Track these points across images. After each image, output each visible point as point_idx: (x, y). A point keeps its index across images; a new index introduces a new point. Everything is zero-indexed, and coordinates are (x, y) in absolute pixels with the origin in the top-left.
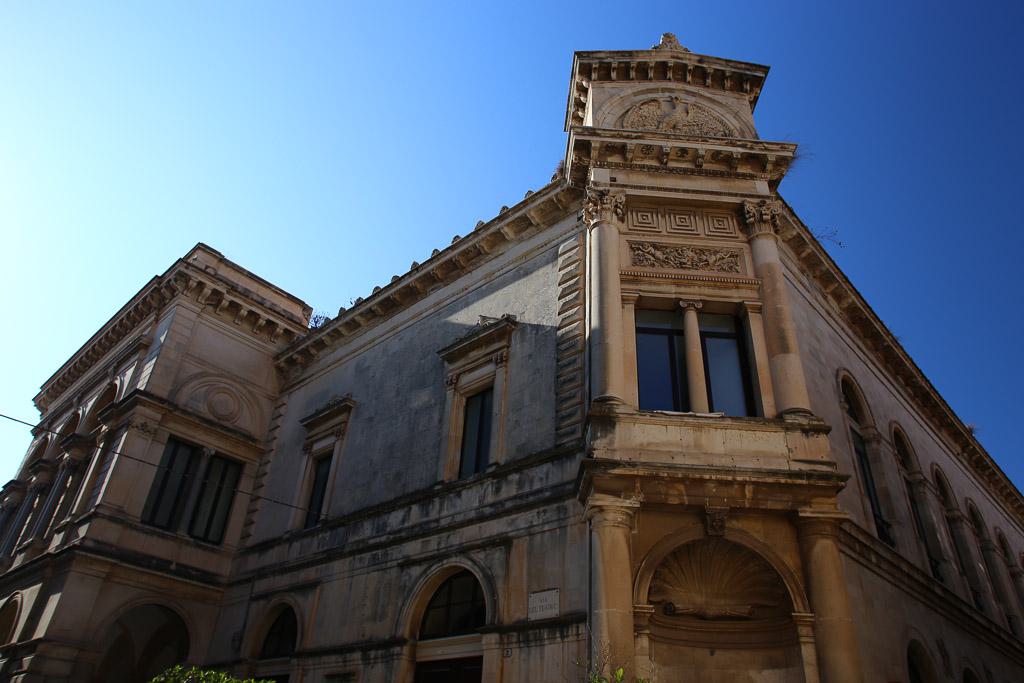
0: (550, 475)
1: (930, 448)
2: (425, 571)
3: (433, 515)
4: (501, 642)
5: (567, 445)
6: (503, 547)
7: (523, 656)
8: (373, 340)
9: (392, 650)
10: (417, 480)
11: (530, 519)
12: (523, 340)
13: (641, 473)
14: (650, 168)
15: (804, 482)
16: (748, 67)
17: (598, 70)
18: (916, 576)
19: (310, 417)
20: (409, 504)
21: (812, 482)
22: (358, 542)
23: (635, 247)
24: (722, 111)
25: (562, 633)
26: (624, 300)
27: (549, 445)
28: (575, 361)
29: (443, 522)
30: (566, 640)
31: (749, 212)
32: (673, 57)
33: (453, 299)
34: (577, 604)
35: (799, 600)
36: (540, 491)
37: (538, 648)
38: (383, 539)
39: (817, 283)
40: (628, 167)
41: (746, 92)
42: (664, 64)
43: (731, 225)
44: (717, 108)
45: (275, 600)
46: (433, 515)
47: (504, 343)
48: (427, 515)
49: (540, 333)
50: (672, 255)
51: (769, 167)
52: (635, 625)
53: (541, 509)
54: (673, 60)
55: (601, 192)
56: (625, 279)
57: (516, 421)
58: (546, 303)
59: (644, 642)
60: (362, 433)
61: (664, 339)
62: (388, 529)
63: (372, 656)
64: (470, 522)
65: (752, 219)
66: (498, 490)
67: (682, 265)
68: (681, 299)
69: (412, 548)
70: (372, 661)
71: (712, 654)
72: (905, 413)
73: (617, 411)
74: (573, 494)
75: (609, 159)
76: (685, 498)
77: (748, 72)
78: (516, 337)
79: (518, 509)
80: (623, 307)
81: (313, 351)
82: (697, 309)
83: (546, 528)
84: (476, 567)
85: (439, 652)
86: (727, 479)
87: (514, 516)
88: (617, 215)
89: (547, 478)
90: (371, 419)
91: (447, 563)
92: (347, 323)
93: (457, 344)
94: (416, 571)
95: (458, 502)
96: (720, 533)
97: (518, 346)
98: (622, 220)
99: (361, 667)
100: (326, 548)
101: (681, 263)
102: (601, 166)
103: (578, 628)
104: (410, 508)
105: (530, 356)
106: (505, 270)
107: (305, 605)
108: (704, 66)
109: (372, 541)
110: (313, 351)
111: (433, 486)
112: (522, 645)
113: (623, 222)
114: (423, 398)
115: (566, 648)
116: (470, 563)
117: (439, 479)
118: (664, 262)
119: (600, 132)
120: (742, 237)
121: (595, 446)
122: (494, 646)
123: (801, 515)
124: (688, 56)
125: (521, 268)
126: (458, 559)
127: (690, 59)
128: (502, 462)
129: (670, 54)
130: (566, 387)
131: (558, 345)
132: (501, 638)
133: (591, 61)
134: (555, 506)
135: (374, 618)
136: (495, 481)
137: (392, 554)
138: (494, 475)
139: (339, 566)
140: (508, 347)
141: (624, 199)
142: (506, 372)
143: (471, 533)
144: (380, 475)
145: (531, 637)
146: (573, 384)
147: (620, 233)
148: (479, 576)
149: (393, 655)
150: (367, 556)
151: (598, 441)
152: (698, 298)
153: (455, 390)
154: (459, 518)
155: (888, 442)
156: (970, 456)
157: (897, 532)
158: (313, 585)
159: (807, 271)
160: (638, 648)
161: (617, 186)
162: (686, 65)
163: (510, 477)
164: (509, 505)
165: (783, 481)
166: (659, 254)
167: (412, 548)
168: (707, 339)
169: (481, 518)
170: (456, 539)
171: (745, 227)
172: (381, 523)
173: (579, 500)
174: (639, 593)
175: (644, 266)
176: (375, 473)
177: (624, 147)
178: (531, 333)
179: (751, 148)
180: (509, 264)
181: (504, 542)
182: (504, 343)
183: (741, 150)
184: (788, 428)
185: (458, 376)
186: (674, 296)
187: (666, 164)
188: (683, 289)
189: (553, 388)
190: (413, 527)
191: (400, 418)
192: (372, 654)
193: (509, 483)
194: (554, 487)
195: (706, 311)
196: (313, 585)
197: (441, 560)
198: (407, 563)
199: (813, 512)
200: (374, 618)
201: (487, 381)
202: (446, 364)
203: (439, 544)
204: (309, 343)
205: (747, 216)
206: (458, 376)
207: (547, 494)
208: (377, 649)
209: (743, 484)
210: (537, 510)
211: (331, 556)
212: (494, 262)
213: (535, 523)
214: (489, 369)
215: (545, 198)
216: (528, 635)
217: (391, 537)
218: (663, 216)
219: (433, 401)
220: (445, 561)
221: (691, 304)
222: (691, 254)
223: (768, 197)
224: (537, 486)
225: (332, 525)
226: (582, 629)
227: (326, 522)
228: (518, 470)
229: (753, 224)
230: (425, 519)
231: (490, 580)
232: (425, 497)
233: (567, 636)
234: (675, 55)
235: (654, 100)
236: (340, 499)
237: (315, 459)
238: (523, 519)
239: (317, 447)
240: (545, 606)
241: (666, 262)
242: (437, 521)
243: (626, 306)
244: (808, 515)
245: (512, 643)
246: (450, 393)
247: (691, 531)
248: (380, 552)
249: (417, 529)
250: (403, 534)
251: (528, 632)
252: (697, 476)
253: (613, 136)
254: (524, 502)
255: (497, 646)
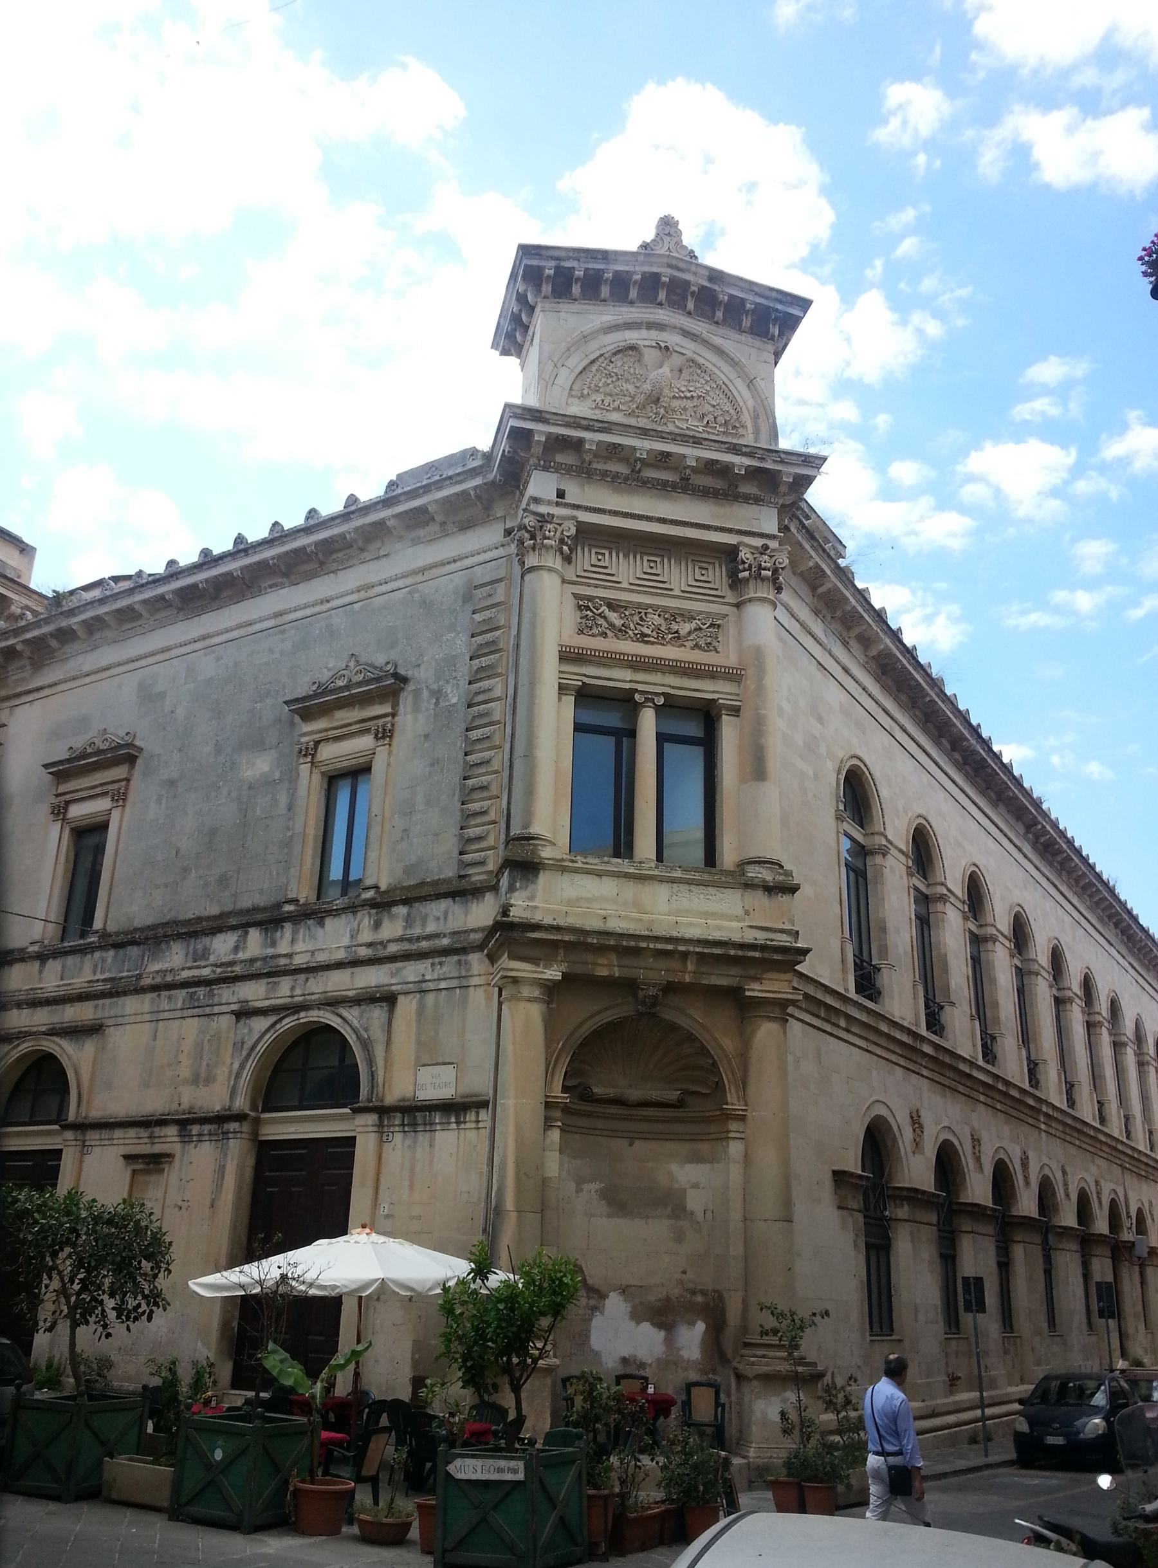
0: (450, 916)
1: (970, 841)
2: (273, 1025)
3: (283, 948)
4: (381, 1125)
5: (474, 879)
6: (384, 1004)
7: (408, 1142)
8: (168, 649)
9: (226, 1126)
10: (255, 891)
11: (422, 972)
12: (416, 709)
13: (567, 938)
14: (616, 476)
15: (757, 954)
16: (780, 297)
17: (553, 279)
18: (898, 1035)
19: (61, 762)
20: (245, 927)
21: (766, 955)
22: (164, 972)
23: (583, 604)
24: (732, 375)
25: (457, 1117)
26: (562, 689)
27: (449, 872)
28: (488, 762)
29: (299, 960)
30: (462, 1126)
31: (743, 562)
32: (670, 266)
33: (308, 612)
34: (478, 1083)
35: (733, 1090)
36: (436, 936)
37: (428, 1134)
38: (206, 972)
39: (835, 625)
40: (585, 473)
41: (772, 338)
42: (656, 277)
43: (717, 576)
44: (726, 368)
45: (26, 1047)
46: (283, 948)
47: (387, 709)
48: (274, 944)
49: (442, 704)
50: (628, 618)
51: (783, 489)
52: (546, 1118)
53: (437, 960)
54: (669, 271)
55: (542, 516)
56: (567, 656)
57: (405, 830)
58: (451, 661)
59: (555, 1135)
60: (159, 801)
61: (610, 741)
62: (212, 959)
63: (194, 1133)
64: (339, 965)
65: (746, 574)
66: (377, 925)
67: (642, 638)
68: (637, 691)
69: (254, 992)
70: (195, 1139)
71: (631, 1145)
72: (942, 794)
73: (544, 854)
74: (480, 947)
75: (559, 458)
76: (616, 969)
77: (779, 307)
78: (406, 701)
79: (407, 957)
80: (560, 700)
81: (54, 643)
82: (657, 708)
83: (443, 985)
84: (346, 1026)
85: (292, 1129)
86: (671, 949)
87: (399, 965)
88: (562, 553)
89: (446, 918)
90: (172, 783)
91: (305, 1017)
92: (119, 611)
93: (315, 695)
94: (260, 1024)
95: (319, 932)
96: (653, 1011)
97: (409, 717)
98: (568, 559)
99: (178, 1146)
100: (107, 975)
101: (644, 635)
102: (546, 469)
103: (478, 1113)
104: (247, 933)
105: (426, 736)
106: (389, 587)
107: (76, 1057)
108: (716, 287)
109: (186, 974)
110: (54, 643)
111: (279, 905)
112: (406, 1129)
113: (570, 563)
114: (261, 765)
115: (462, 1139)
116: (339, 1020)
117: (291, 896)
118: (620, 630)
119: (548, 416)
120: (730, 597)
121: (512, 902)
122: (371, 1129)
123: (747, 993)
124: (693, 268)
125: (417, 591)
126: (321, 1013)
127: (695, 274)
128: (383, 887)
129: (665, 260)
130: (475, 796)
131: (467, 730)
132: (380, 1119)
133: (542, 263)
134: (456, 958)
135: (195, 1081)
136: (374, 911)
137: (220, 995)
138: (372, 904)
139: (131, 1004)
140: (394, 715)
141: (573, 530)
142: (390, 754)
143: (339, 982)
144: (193, 875)
145: (419, 1120)
146: (485, 794)
147: (564, 581)
148: (351, 1038)
149: (228, 1133)
150: (181, 994)
151: (516, 894)
152: (659, 690)
153: (312, 763)
154: (322, 958)
155: (901, 851)
156: (1037, 837)
157: (886, 979)
158: (94, 1030)
159: (824, 612)
160: (548, 1142)
161: (567, 505)
162: (688, 284)
163: (395, 910)
164: (393, 948)
165: (732, 952)
166: (613, 617)
167: (254, 992)
168: (666, 744)
169: (356, 963)
170: (318, 986)
171: (736, 583)
172: (200, 947)
173: (487, 955)
174: (553, 1074)
175: (593, 636)
176: (186, 870)
177: (581, 442)
178: (428, 702)
179: (762, 459)
180: (397, 578)
181: (389, 999)
182: (387, 709)
183: (747, 461)
184: (749, 886)
185: (317, 743)
186: (627, 686)
187: (639, 472)
188: (640, 676)
189: (457, 792)
190: (252, 961)
191: (225, 791)
192: (195, 1129)
193: (392, 917)
194: (453, 933)
195: (670, 707)
196: (94, 1030)
197: (297, 1012)
198: (244, 1013)
199: (762, 991)
200: (195, 1081)
201: (362, 760)
202: (297, 719)
203: (293, 989)
204: (47, 629)
205: (741, 567)
206: (317, 743)
207: (445, 941)
208: (201, 1124)
209: (685, 955)
210: (430, 961)
211: (116, 991)
212: (373, 566)
213: (427, 978)
214: (365, 742)
215: (458, 488)
216: (415, 1117)
217: (219, 970)
218: (626, 556)
219: (277, 775)
220: (302, 1014)
221: (649, 698)
222: (657, 620)
223: (773, 537)
224: (431, 928)
225: (119, 942)
226: (484, 1115)
227: (104, 934)
228: (406, 902)
229: (747, 580)
230: (270, 951)
231: (366, 1045)
232: (270, 919)
233: (465, 1122)
234: (674, 262)
235: (633, 348)
236: (123, 903)
237: (73, 830)
238: (412, 971)
239: (75, 811)
240: (436, 1084)
241: (621, 632)
242: (290, 956)
243: (564, 698)
244: (756, 994)
245: (394, 1126)
246: (305, 769)
247: (619, 1010)
248: (201, 991)
249: (258, 964)
250: (237, 969)
251: (415, 1114)
252: (633, 944)
253: (567, 425)
254: (414, 947)
255: (375, 1129)
